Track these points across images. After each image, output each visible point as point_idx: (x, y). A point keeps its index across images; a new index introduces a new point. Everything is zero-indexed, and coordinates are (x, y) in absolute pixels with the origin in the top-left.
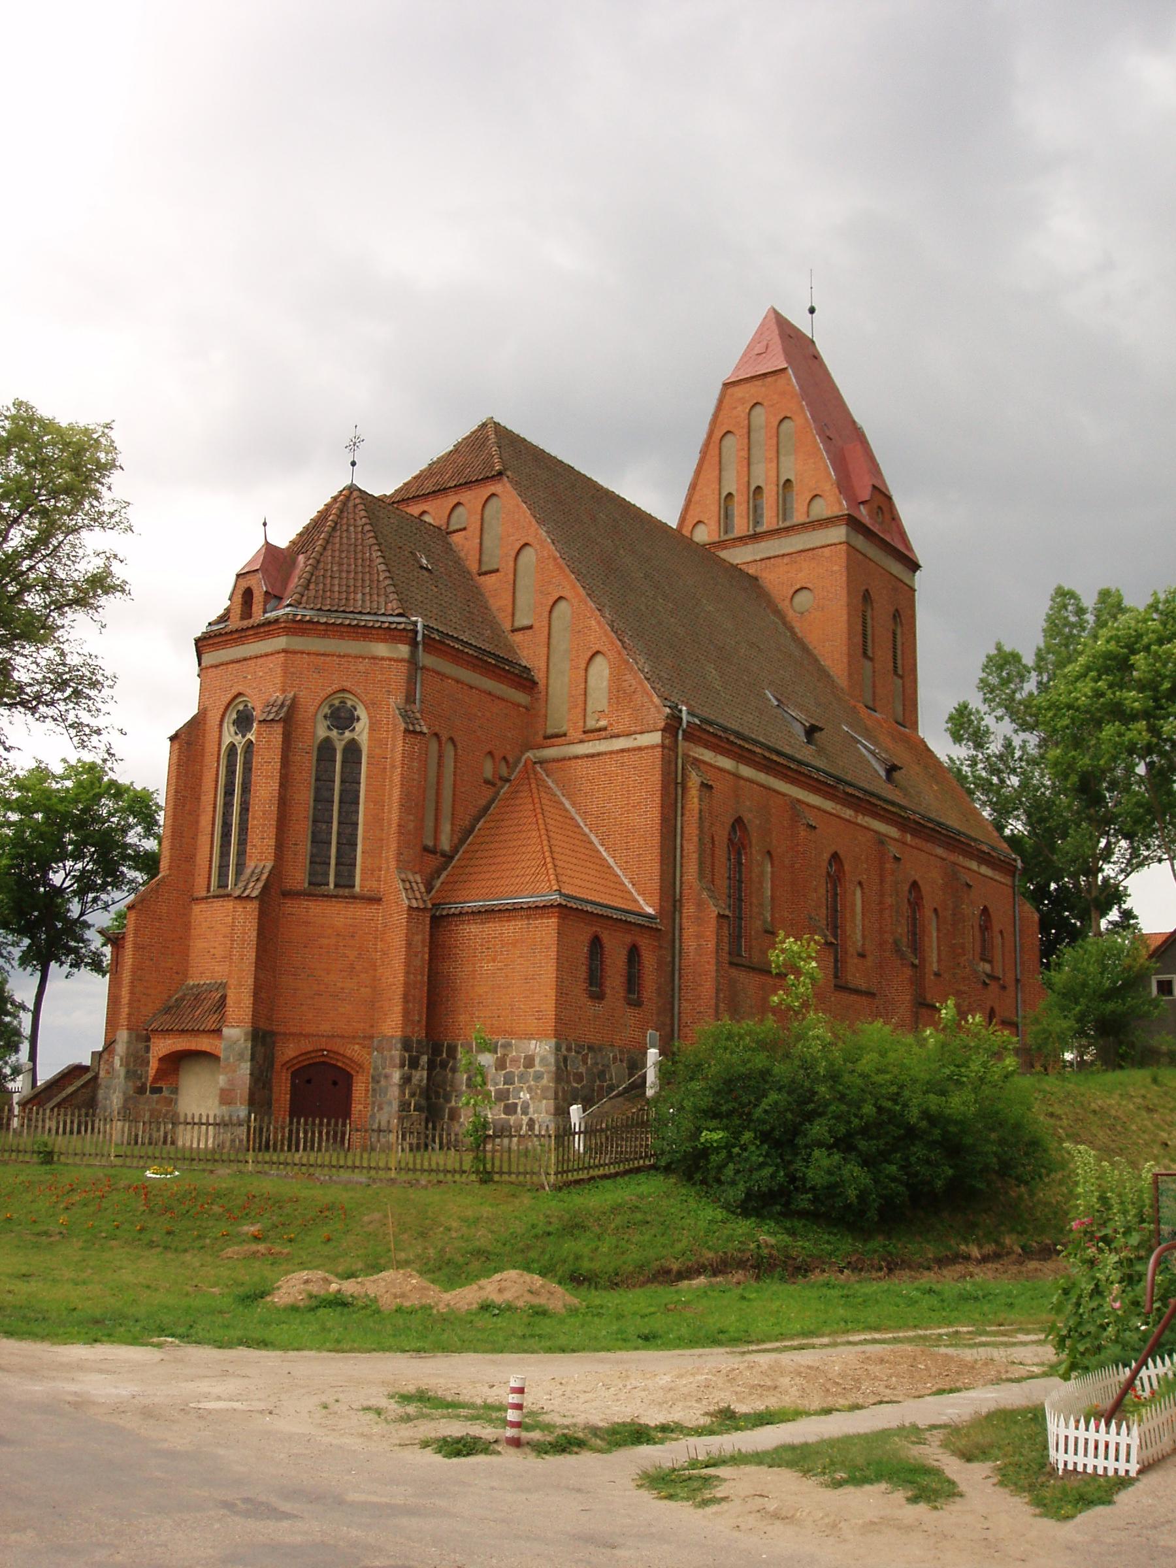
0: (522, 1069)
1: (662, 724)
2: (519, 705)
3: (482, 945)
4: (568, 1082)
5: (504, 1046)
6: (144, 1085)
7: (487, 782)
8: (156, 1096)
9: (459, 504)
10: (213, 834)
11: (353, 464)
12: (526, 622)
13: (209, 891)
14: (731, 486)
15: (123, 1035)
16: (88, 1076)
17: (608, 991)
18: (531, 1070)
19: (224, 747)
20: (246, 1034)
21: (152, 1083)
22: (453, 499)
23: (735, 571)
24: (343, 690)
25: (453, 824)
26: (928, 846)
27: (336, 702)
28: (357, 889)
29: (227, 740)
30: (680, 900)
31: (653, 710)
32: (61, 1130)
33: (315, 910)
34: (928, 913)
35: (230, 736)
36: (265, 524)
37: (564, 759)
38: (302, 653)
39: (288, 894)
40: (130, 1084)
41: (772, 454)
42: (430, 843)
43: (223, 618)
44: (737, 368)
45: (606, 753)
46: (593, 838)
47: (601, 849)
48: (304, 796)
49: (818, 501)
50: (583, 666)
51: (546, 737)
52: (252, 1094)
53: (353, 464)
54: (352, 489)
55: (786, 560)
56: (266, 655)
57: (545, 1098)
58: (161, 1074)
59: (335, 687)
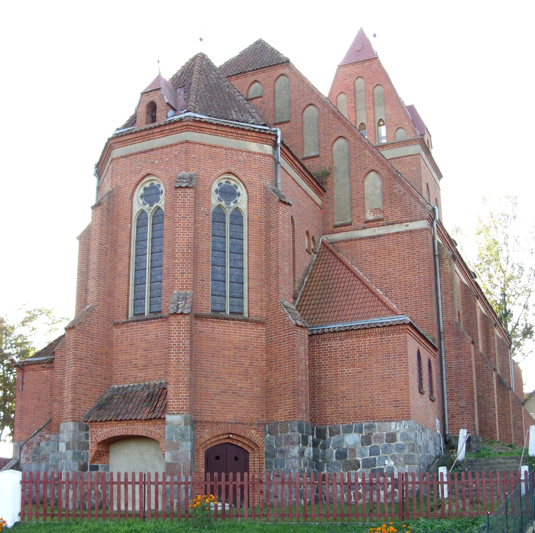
0: (385, 443)
6: (86, 464)
8: (94, 473)
12: (313, 154)
13: (127, 318)
20: (185, 419)
27: (224, 181)
31: (419, 206)
32: (239, 490)
38: (200, 144)
41: (371, 105)
43: (133, 121)
56: (171, 146)
57: (407, 464)
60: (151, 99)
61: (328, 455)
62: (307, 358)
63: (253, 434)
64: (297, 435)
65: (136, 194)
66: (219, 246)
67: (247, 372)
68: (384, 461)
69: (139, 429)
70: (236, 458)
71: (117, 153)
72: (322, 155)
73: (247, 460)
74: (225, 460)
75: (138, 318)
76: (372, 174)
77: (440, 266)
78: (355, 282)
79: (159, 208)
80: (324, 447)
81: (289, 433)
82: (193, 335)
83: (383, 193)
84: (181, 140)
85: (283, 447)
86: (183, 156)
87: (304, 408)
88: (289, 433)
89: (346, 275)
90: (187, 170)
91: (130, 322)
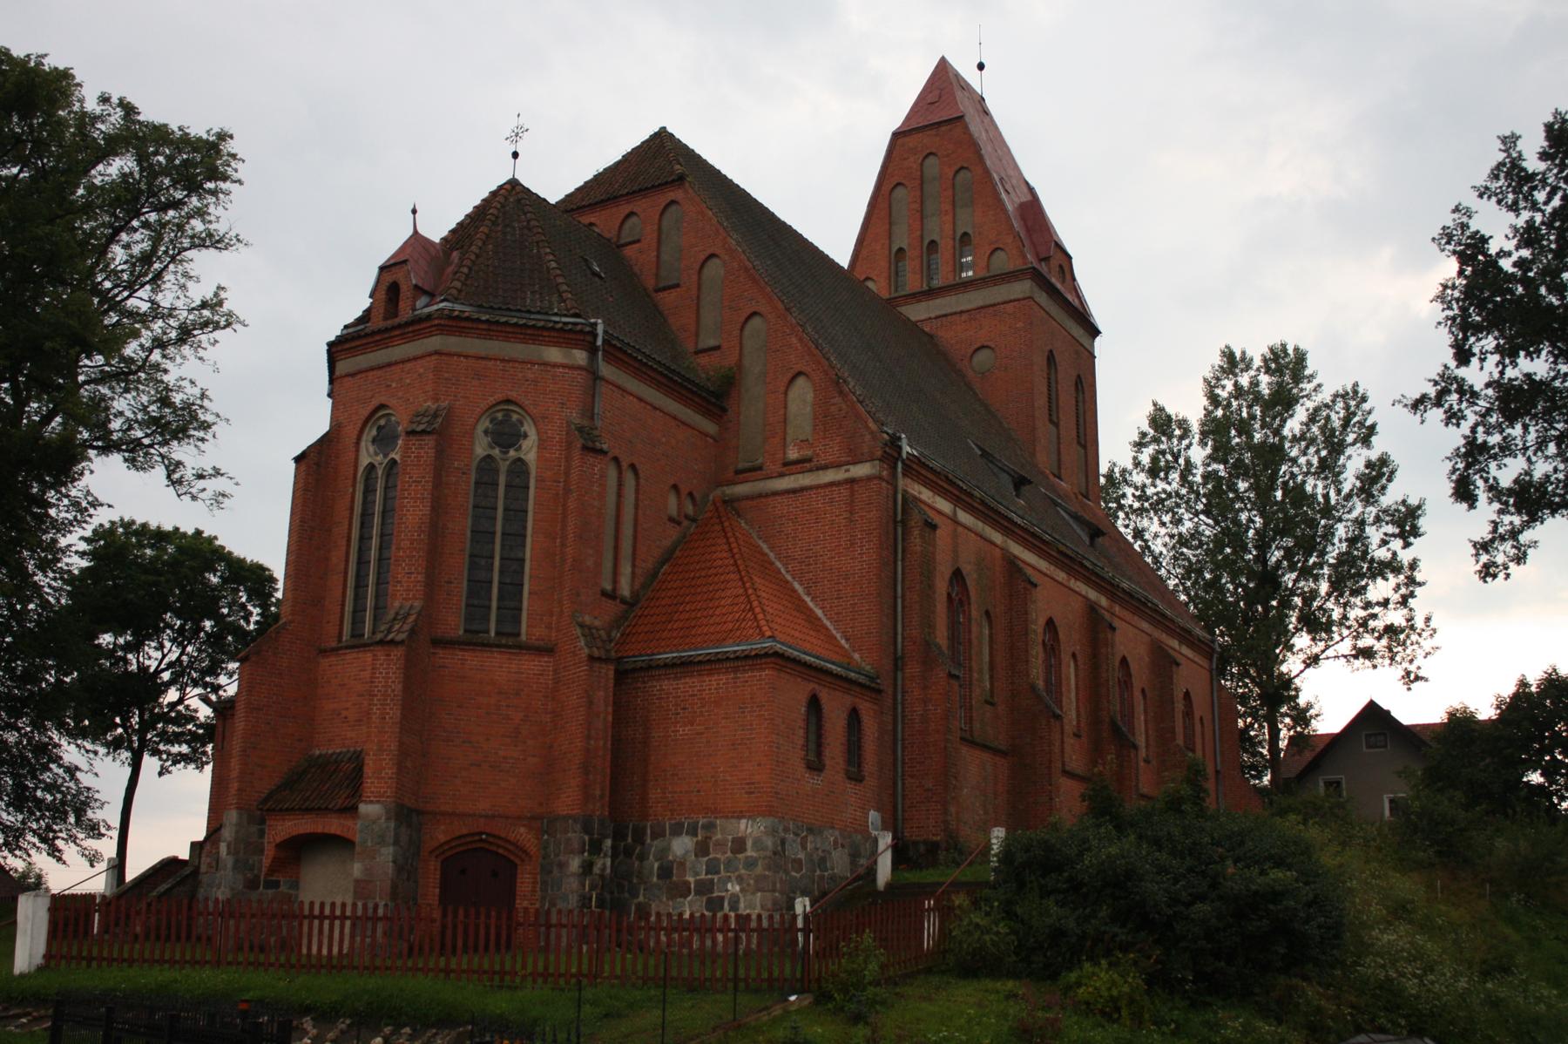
0: (729, 854)
1: (879, 453)
2: (707, 435)
4: (786, 872)
6: (257, 877)
7: (671, 519)
8: (270, 892)
9: (632, 214)
10: (346, 573)
11: (515, 155)
12: (712, 343)
13: (340, 641)
14: (902, 240)
15: (232, 817)
16: (187, 871)
17: (827, 762)
18: (740, 856)
19: (361, 469)
22: (625, 209)
23: (914, 327)
24: (508, 401)
25: (634, 566)
26: (1136, 620)
27: (500, 416)
28: (524, 637)
29: (365, 461)
30: (902, 658)
31: (868, 437)
33: (472, 660)
34: (1137, 694)
36: (414, 212)
37: (760, 496)
38: (459, 355)
39: (438, 642)
41: (948, 207)
42: (608, 587)
45: (811, 488)
46: (797, 586)
47: (808, 599)
48: (461, 525)
49: (999, 254)
50: (782, 389)
51: (738, 472)
52: (394, 887)
53: (515, 155)
54: (513, 184)
55: (964, 317)
56: (415, 359)
58: (278, 865)
59: (499, 396)
62: (610, 709)
63: (522, 834)
64: (575, 836)
65: (364, 437)
74: (472, 880)
77: (904, 540)
84: (431, 349)
85: (562, 858)
87: (598, 793)
90: (436, 400)
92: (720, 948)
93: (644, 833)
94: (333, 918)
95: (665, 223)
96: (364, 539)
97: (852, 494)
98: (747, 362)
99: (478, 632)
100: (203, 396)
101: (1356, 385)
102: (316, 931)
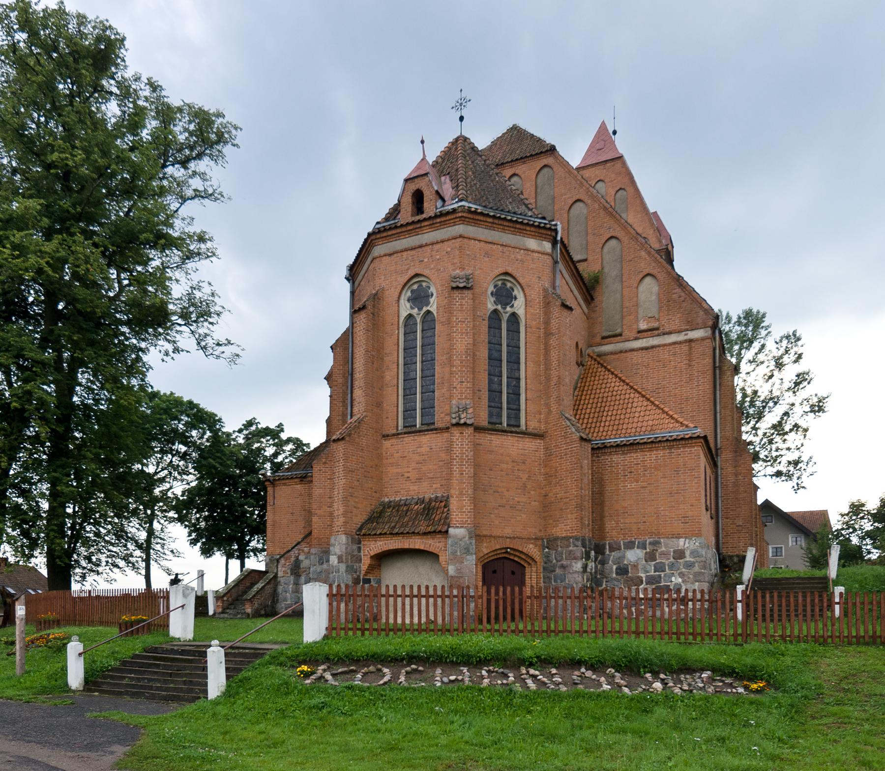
0: (672, 560)
3: (624, 470)
5: (653, 544)
6: (359, 576)
8: (366, 586)
11: (462, 119)
19: (402, 319)
21: (365, 575)
27: (500, 283)
28: (523, 427)
29: (404, 314)
31: (702, 313)
35: (405, 309)
36: (422, 142)
40: (350, 576)
44: (584, 159)
45: (659, 346)
53: (462, 119)
56: (442, 241)
58: (371, 569)
60: (417, 187)
61: (607, 571)
63: (531, 549)
64: (579, 550)
65: (403, 297)
66: (495, 355)
67: (525, 486)
68: (670, 577)
69: (417, 543)
70: (513, 573)
71: (378, 250)
72: (590, 258)
73: (523, 575)
75: (409, 429)
76: (648, 280)
77: (720, 378)
78: (632, 395)
79: (428, 312)
80: (603, 563)
81: (571, 548)
82: (476, 446)
83: (660, 300)
85: (564, 562)
86: (457, 252)
88: (571, 548)
89: (621, 388)
91: (401, 434)
92: (666, 616)
93: (605, 548)
94: (443, 597)
95: (539, 180)
96: (409, 363)
97: (690, 348)
98: (606, 270)
99: (495, 424)
100: (213, 295)
101: (795, 332)
102: (391, 609)
